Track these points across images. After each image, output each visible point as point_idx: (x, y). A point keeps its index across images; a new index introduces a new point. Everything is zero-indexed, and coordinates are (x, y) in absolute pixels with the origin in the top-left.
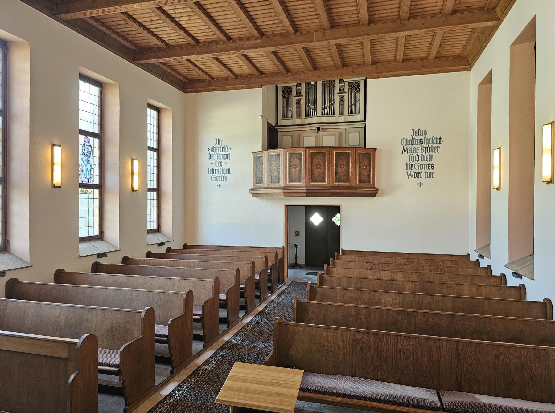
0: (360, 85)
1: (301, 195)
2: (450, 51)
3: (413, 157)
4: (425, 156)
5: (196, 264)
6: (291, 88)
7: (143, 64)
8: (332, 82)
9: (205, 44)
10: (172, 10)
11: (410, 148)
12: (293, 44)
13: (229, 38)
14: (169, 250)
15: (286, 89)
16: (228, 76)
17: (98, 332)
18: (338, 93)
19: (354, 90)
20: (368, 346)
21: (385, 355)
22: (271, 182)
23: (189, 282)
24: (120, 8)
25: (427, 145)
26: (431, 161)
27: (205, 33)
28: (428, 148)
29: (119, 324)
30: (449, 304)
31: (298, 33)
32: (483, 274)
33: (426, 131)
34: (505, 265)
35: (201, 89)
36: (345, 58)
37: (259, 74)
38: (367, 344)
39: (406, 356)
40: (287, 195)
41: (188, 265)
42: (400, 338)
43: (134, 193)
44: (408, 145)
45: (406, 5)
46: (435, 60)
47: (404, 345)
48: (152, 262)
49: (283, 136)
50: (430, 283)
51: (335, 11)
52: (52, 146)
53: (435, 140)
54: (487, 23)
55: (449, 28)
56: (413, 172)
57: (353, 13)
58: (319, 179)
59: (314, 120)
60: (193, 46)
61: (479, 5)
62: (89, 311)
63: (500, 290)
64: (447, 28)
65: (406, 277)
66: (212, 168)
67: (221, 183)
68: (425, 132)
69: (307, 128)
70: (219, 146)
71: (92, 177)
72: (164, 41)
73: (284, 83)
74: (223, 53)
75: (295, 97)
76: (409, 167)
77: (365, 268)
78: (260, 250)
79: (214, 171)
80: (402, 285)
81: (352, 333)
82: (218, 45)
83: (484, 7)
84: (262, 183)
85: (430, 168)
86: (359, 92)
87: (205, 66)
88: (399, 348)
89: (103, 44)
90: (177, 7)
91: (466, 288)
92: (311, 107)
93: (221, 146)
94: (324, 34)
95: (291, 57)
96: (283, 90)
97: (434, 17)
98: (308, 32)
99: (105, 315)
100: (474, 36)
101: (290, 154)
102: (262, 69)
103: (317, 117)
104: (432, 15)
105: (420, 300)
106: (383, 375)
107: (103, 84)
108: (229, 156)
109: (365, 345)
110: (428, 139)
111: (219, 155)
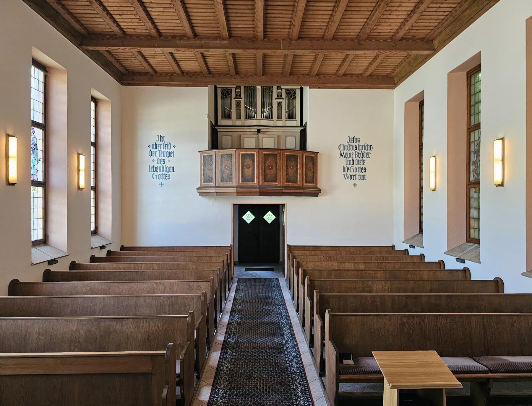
5: (160, 266)
6: (230, 90)
7: (89, 51)
9: (168, 38)
11: (346, 153)
12: (260, 49)
13: (195, 35)
14: (109, 252)
16: (174, 72)
17: (131, 343)
18: (276, 99)
22: (222, 181)
23: (182, 284)
25: (361, 151)
26: (364, 165)
28: (361, 153)
29: (157, 332)
30: (428, 287)
31: (265, 40)
32: (418, 261)
35: (141, 82)
36: (294, 67)
37: (207, 73)
41: (151, 268)
43: (80, 191)
47: (442, 323)
48: (107, 267)
49: (222, 136)
51: (309, 24)
52: (6, 136)
53: (367, 147)
54: (425, 51)
58: (271, 179)
59: (254, 122)
60: (154, 38)
62: (117, 322)
63: (451, 273)
64: (395, 52)
66: (154, 166)
67: (164, 181)
69: (247, 130)
70: (161, 143)
71: (37, 173)
72: (122, 29)
75: (234, 98)
77: (322, 261)
79: (155, 169)
80: (375, 274)
81: (399, 317)
83: (425, 38)
84: (212, 182)
85: (363, 171)
87: (153, 59)
88: (438, 326)
89: (54, 24)
91: (425, 273)
93: (163, 143)
96: (222, 91)
97: (386, 41)
98: (275, 40)
100: (407, 61)
101: (242, 154)
102: (213, 68)
103: (256, 119)
104: (384, 39)
105: (405, 285)
107: (47, 68)
108: (173, 153)
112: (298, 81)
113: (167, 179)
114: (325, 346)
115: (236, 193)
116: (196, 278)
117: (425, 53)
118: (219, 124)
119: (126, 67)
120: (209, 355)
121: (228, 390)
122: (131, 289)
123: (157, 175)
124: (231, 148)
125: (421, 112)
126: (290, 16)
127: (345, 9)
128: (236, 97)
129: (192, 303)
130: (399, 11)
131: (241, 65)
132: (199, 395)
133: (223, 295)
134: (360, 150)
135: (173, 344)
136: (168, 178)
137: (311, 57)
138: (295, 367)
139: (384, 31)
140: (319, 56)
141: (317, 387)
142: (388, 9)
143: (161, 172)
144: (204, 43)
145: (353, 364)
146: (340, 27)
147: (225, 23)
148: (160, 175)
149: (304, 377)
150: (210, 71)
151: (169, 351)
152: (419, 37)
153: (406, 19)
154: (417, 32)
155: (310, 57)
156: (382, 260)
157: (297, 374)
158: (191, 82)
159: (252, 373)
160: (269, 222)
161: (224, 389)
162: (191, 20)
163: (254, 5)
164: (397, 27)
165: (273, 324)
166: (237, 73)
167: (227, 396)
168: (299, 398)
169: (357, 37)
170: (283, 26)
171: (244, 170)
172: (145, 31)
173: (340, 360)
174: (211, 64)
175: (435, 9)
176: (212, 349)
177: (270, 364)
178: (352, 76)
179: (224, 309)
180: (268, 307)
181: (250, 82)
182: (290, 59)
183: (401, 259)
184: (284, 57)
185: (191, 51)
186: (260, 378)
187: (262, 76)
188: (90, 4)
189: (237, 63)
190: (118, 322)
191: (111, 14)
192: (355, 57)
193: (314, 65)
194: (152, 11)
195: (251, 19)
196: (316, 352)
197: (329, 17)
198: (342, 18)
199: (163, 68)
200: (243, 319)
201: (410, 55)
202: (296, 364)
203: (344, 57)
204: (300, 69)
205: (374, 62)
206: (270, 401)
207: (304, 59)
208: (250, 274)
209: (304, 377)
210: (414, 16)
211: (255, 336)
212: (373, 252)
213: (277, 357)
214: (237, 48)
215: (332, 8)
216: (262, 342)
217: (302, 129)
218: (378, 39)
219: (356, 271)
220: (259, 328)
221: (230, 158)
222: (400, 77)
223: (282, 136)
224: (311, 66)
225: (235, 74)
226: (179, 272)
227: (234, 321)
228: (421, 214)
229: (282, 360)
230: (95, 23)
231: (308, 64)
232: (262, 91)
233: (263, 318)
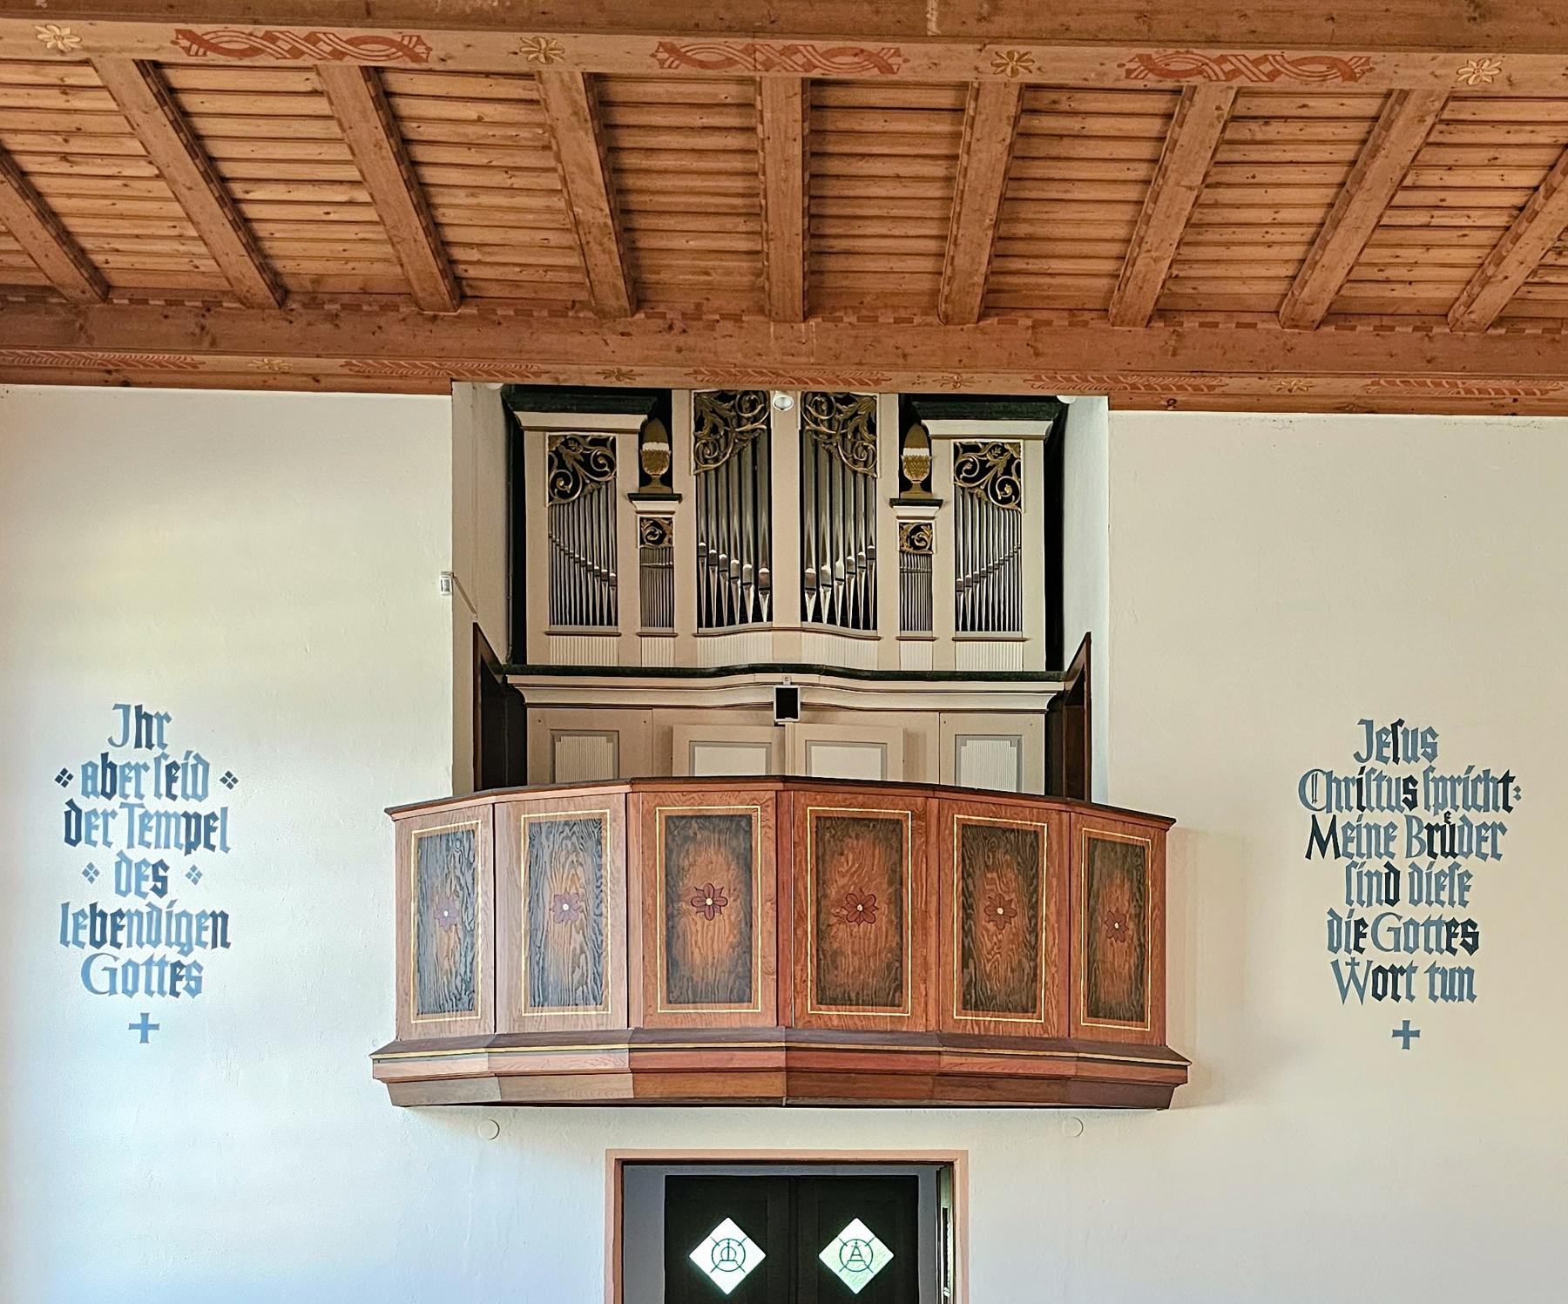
0: (1019, 464)
1: (757, 1086)
3: (1365, 879)
4: (1429, 876)
12: (782, 33)
16: (225, 285)
19: (985, 490)
22: (539, 998)
25: (1442, 813)
26: (1464, 903)
33: (1434, 735)
44: (1339, 808)
46: (1491, 331)
53: (1481, 787)
56: (1369, 963)
58: (864, 985)
59: (752, 646)
66: (93, 907)
67: (159, 1007)
68: (1430, 739)
69: (711, 694)
70: (145, 756)
74: (261, 30)
85: (1456, 942)
86: (1011, 505)
87: (64, 168)
93: (158, 761)
95: (696, 183)
102: (474, 255)
108: (218, 824)
110: (1442, 779)
111: (142, 817)
112: (1037, 354)
113: (184, 994)
123: (112, 964)
128: (646, 490)
134: (1438, 807)
136: (187, 988)
143: (141, 944)
148: (136, 966)
150: (458, 280)
160: (856, 1282)
166: (639, 296)
184: (943, 150)
187: (805, 319)
192: (1427, 155)
204: (1056, 265)
217: (1060, 696)
221: (591, 844)
223: (932, 740)
225: (625, 302)
231: (1100, 213)
232: (809, 448)
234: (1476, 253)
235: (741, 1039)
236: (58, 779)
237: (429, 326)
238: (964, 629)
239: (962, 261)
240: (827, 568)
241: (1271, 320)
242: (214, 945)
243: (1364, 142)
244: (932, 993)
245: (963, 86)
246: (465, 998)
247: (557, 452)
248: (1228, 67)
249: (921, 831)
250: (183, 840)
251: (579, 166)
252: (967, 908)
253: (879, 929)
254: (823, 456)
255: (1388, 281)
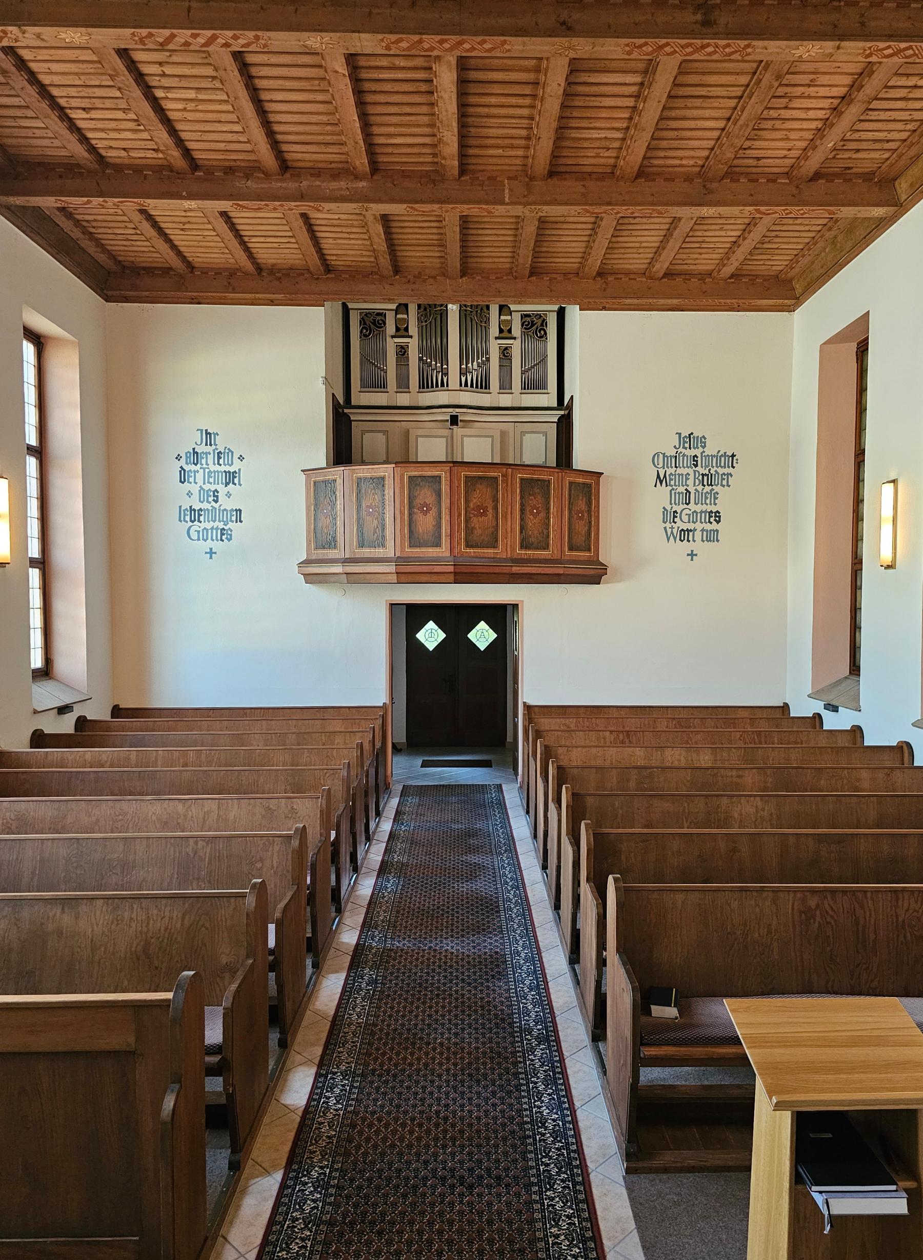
0: (546, 322)
1: (443, 578)
2: (764, 264)
3: (677, 495)
4: (702, 494)
5: (203, 756)
6: (382, 315)
7: (13, 208)
8: (482, 309)
9: (213, 173)
10: (158, 66)
13: (285, 166)
14: (81, 722)
15: (368, 315)
16: (237, 267)
18: (496, 338)
20: (835, 921)
21: (872, 936)
22: (361, 545)
24: (20, 35)
25: (707, 469)
26: (715, 504)
27: (225, 144)
33: (705, 439)
34: (915, 722)
38: (832, 917)
39: (916, 933)
40: (405, 577)
41: (181, 761)
42: (903, 897)
44: (668, 467)
45: (732, 145)
48: (70, 758)
49: (363, 432)
50: (795, 770)
51: (574, 134)
53: (723, 459)
54: (876, 209)
55: (630, 211)
56: (678, 527)
57: (611, 146)
58: (483, 540)
59: (441, 397)
60: (178, 173)
61: (867, 168)
62: (63, 909)
64: (626, 210)
65: (718, 758)
67: (216, 545)
68: (703, 440)
69: (424, 416)
70: (209, 449)
72: (95, 148)
73: (385, 299)
74: (263, 203)
75: (393, 337)
76: (670, 517)
78: (325, 715)
79: (195, 515)
82: (249, 182)
85: (712, 520)
86: (544, 339)
87: (182, 232)
88: (900, 919)
90: (175, 59)
92: (433, 367)
93: (214, 451)
94: (528, 186)
96: (363, 318)
97: (774, 181)
98: (489, 178)
99: (120, 913)
100: (828, 235)
101: (411, 478)
102: (334, 258)
103: (448, 390)
104: (771, 176)
106: (872, 981)
109: (828, 920)
111: (208, 472)
113: (225, 540)
114: (605, 965)
115: (395, 576)
116: (288, 788)
117: (873, 213)
118: (353, 403)
119: (114, 253)
120: (315, 985)
121: (358, 1075)
122: (121, 817)
123: (198, 529)
124: (387, 462)
125: (862, 368)
126: (526, 112)
127: (669, 92)
128: (398, 334)
129: (270, 853)
130: (809, 97)
131: (408, 248)
132: (281, 1091)
133: (360, 828)
134: (706, 467)
135: (192, 973)
136: (227, 538)
137: (583, 226)
138: (533, 1015)
139: (770, 153)
140: (603, 224)
141: (585, 1068)
142: (781, 91)
143: (209, 522)
144: (309, 186)
145: (676, 1018)
146: (656, 142)
147: (359, 131)
148: (207, 530)
149: (553, 1041)
150: (327, 265)
151: (182, 995)
152: (860, 170)
153: (828, 119)
154: (855, 156)
155: (579, 226)
156: (757, 741)
157: (535, 1033)
158: (281, 294)
159: (422, 1030)
160: (482, 646)
161: (346, 1075)
162: (271, 122)
163: (432, 81)
164: (804, 144)
165: (482, 900)
166: (397, 270)
167: (354, 1093)
168: (540, 1099)
169: (700, 171)
170: (507, 142)
171: (415, 516)
172: (155, 155)
173: (642, 1007)
174: (328, 245)
175: (902, 93)
176: (326, 967)
177: (470, 1007)
178: (687, 277)
179: (362, 863)
180: (473, 859)
181: (431, 292)
182: (530, 230)
183: (805, 739)
185: (275, 209)
186: (441, 1044)
187: (461, 277)
188: (4, 77)
189: (396, 242)
190: (66, 909)
191: (62, 109)
192: (696, 227)
193: (591, 248)
194: (167, 98)
195: (425, 119)
196: (585, 974)
197: (627, 116)
198: (661, 119)
199: (207, 255)
200: (408, 888)
201: (837, 221)
202: (534, 1006)
203: (667, 226)
205: (744, 239)
206: (462, 1106)
207: (566, 232)
208: (433, 775)
209: (553, 1041)
210: (848, 111)
211: (436, 933)
212: (733, 722)
213: (488, 987)
214: (393, 201)
215: (633, 89)
216: (452, 947)
218: (755, 176)
219: (690, 771)
220: (448, 912)
221: (380, 486)
222: (808, 280)
223: (511, 435)
224: (582, 250)
225: (391, 273)
226: (247, 773)
227: (386, 894)
228: (855, 627)
229: (500, 995)
230: (23, 133)
233: (458, 885)
234: (719, 255)
235: (437, 560)
236: (177, 458)
237: (316, 282)
238: (525, 389)
239: (521, 260)
240: (470, 365)
241: (642, 277)
242: (237, 522)
243: (672, 223)
244: (509, 543)
245: (518, 217)
246: (333, 544)
247: (363, 318)
248: (615, 211)
249: (505, 481)
250: (224, 481)
251: (376, 234)
252: (522, 510)
253: (489, 519)
254: (469, 319)
255: (686, 264)
